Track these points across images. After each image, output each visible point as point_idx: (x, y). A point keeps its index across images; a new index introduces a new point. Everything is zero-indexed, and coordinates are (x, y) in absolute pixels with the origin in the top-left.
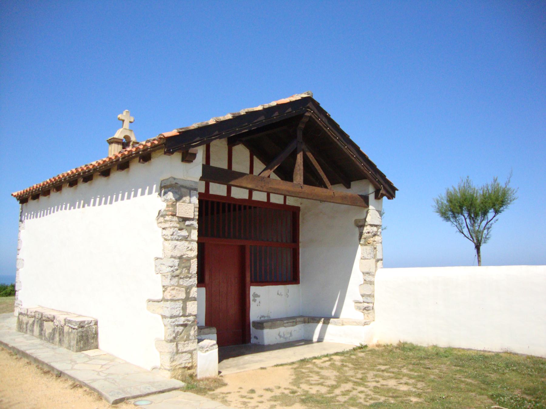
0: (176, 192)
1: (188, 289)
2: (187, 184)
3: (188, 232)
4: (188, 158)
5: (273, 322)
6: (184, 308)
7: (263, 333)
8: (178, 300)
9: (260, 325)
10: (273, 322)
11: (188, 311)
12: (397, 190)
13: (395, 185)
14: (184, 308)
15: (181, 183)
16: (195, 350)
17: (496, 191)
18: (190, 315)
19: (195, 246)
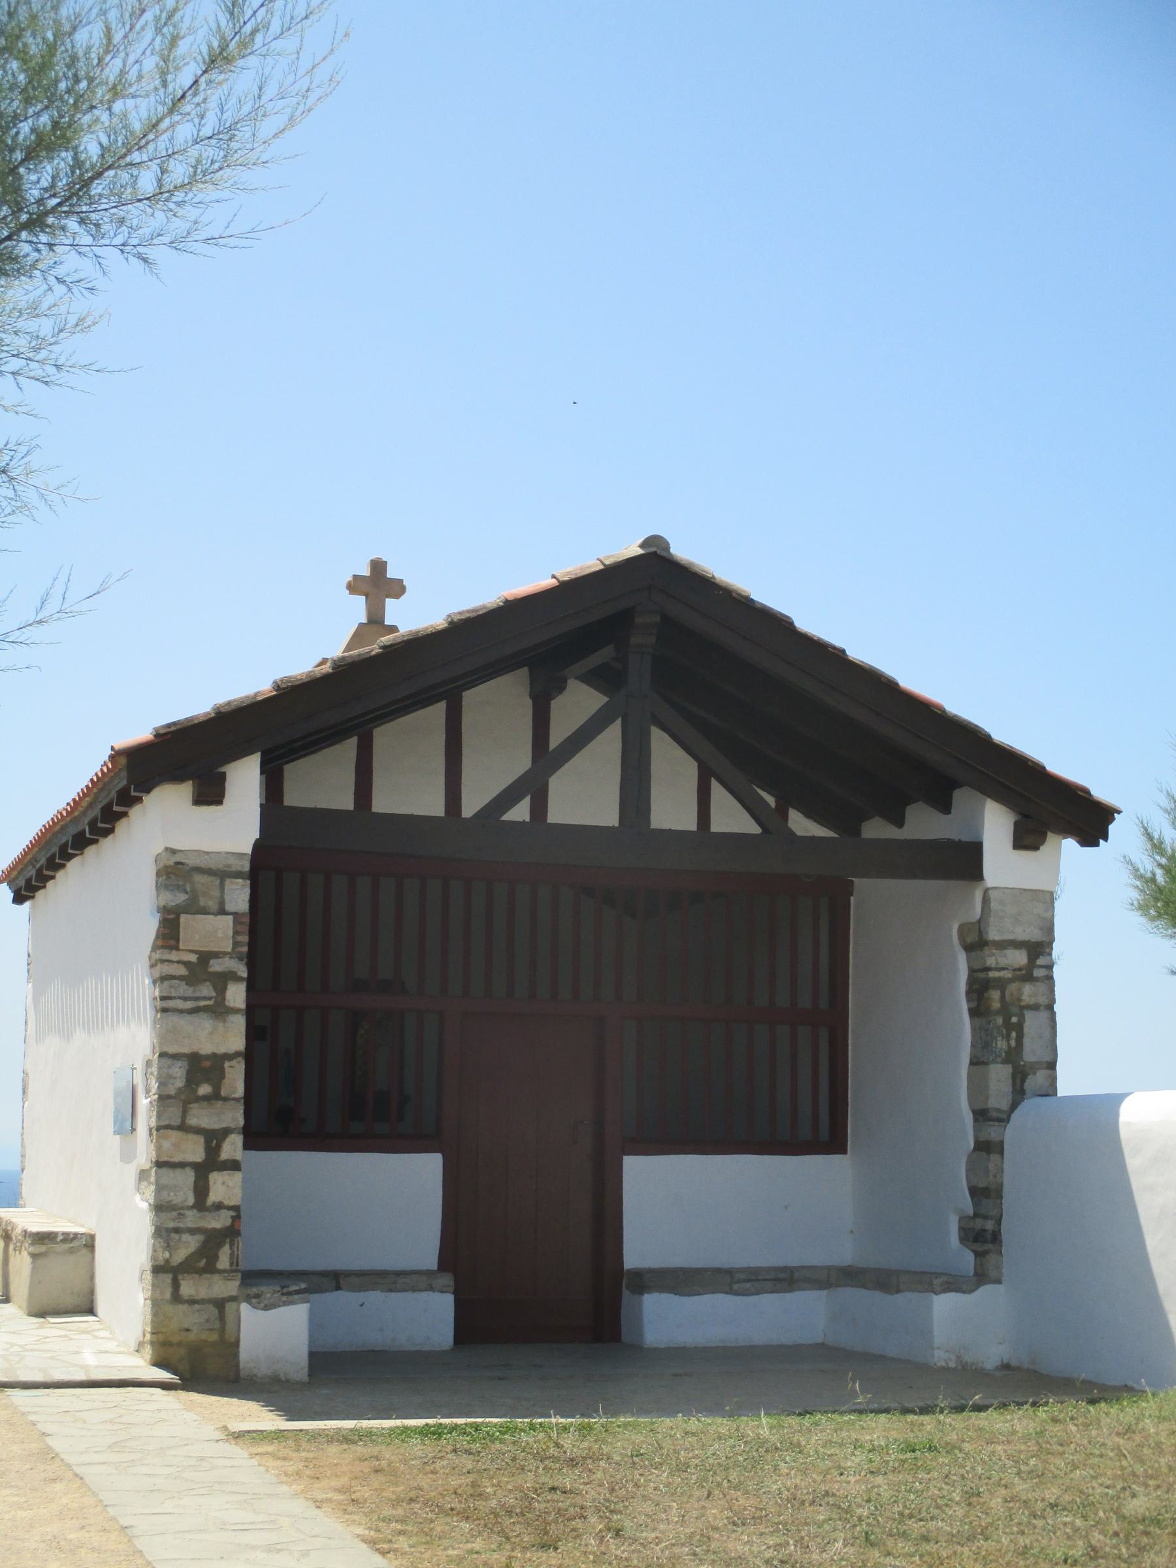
0: (178, 887)
1: (213, 1139)
2: (213, 864)
3: (215, 989)
4: (210, 793)
5: (682, 1281)
6: (201, 1190)
7: (640, 1303)
8: (182, 1165)
9: (645, 1281)
10: (682, 1281)
11: (213, 1197)
12: (1119, 812)
13: (1101, 793)
14: (201, 1190)
15: (191, 861)
16: (233, 1299)
17: (1035, 847)
18: (219, 1206)
19: (239, 1023)
